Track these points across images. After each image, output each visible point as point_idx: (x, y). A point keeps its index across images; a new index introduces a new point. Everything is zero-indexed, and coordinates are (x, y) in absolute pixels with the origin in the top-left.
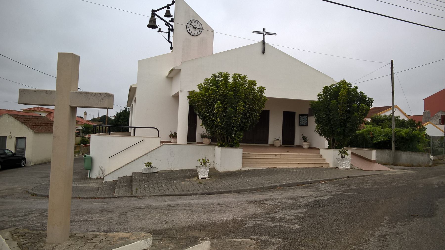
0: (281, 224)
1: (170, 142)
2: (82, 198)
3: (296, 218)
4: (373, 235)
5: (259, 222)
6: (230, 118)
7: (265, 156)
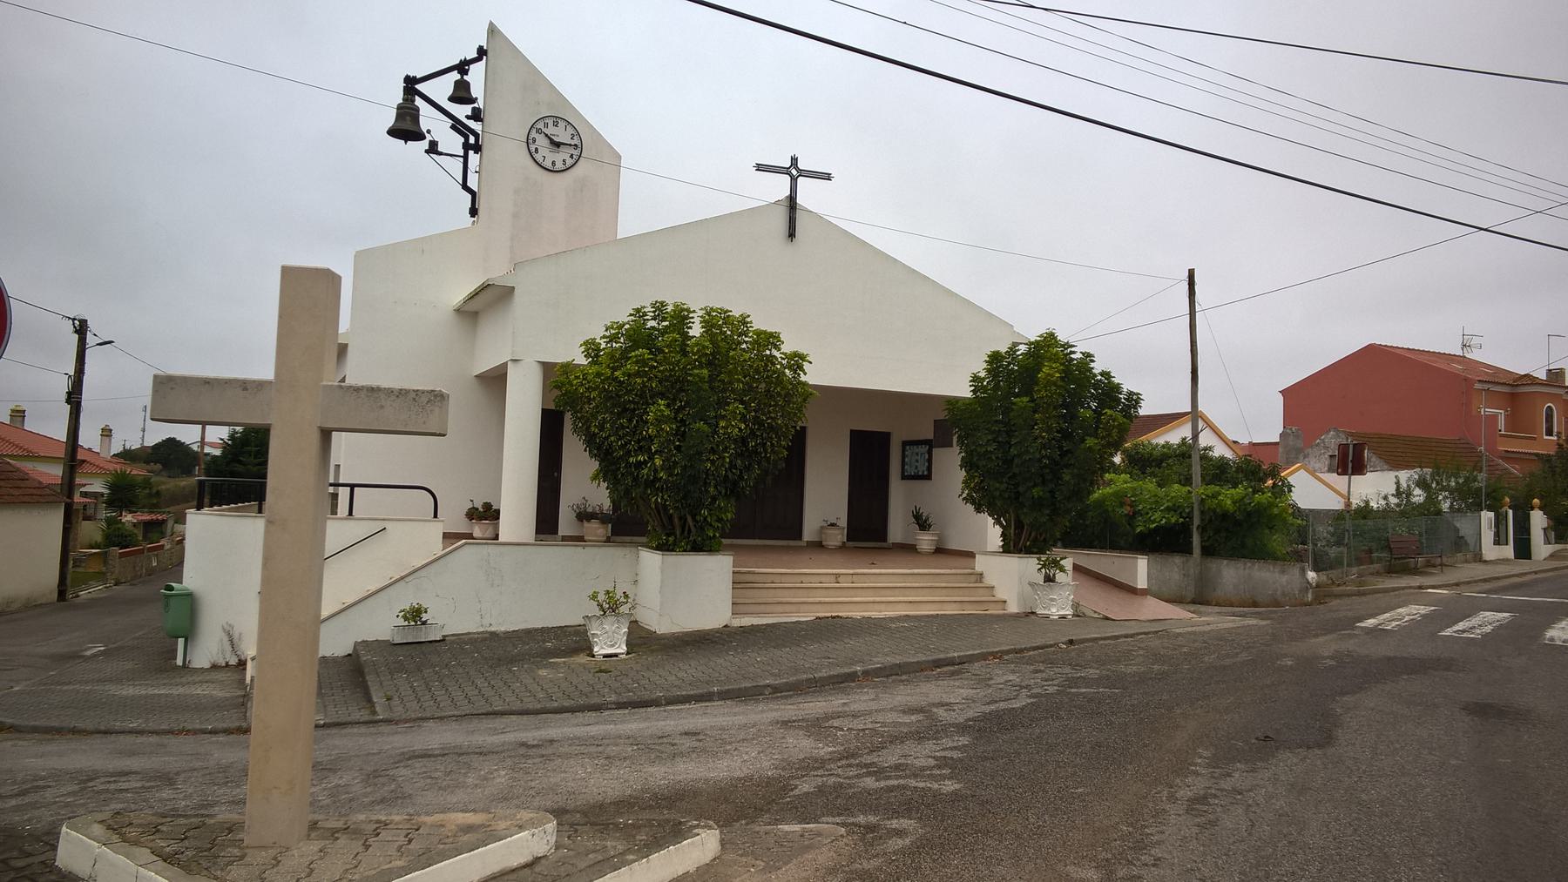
0: (902, 782)
1: (470, 536)
2: (195, 732)
3: (943, 762)
4: (1172, 798)
5: (833, 780)
6: (700, 453)
7: (804, 578)
